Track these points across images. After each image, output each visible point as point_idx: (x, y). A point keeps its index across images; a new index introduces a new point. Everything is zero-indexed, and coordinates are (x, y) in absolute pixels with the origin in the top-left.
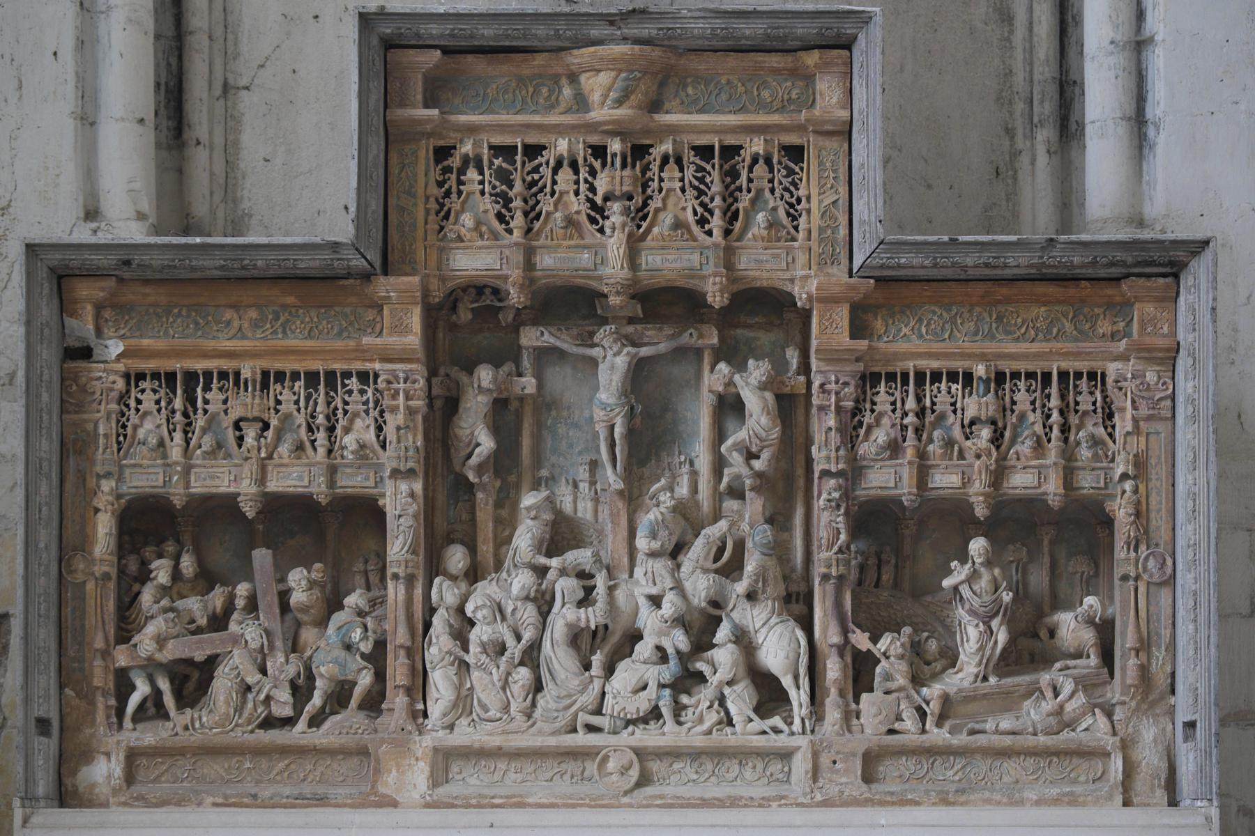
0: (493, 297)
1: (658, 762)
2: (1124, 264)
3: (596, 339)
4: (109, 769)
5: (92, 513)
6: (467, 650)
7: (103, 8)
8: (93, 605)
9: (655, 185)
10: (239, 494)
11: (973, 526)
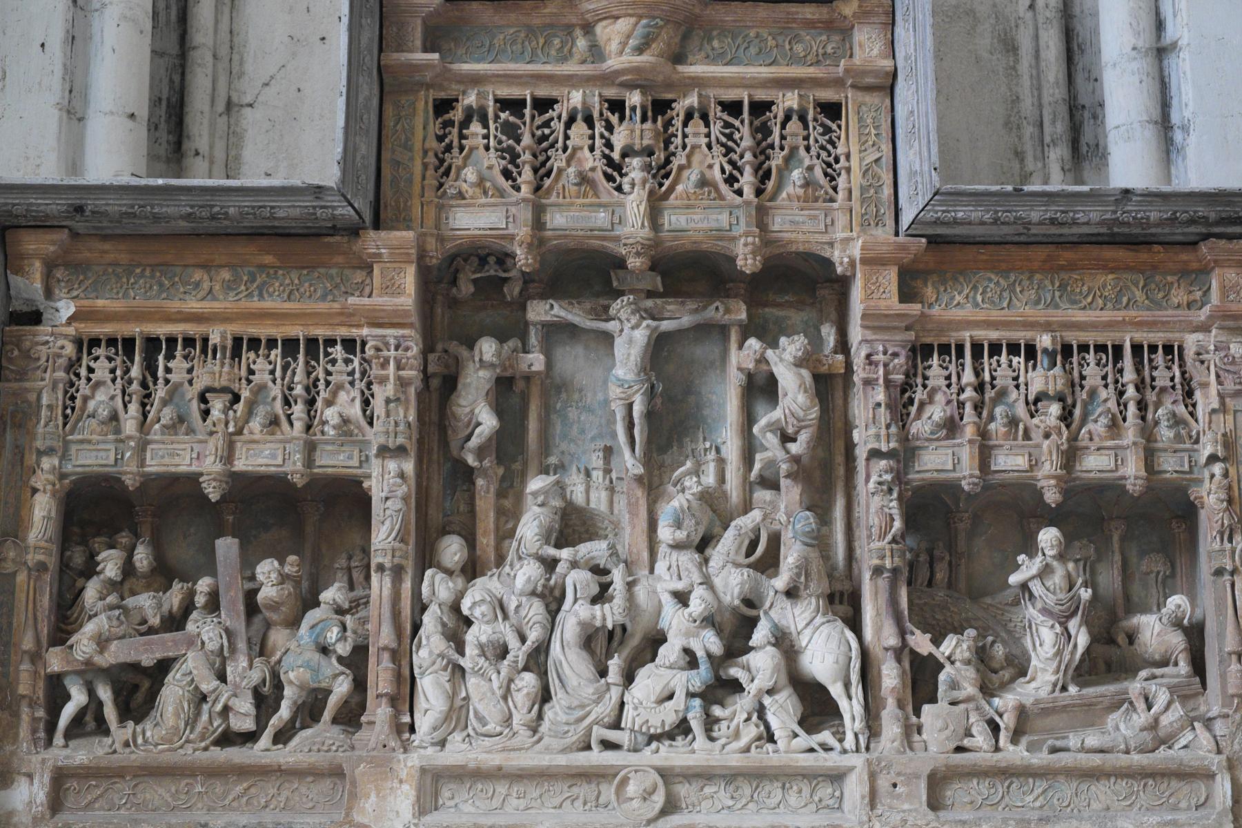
0: (497, 267)
1: (687, 785)
2: (1205, 221)
3: (612, 312)
4: (31, 793)
5: (29, 494)
6: (462, 654)
7: (98, 6)
8: (24, 599)
9: (678, 141)
10: (201, 474)
11: (1034, 520)
